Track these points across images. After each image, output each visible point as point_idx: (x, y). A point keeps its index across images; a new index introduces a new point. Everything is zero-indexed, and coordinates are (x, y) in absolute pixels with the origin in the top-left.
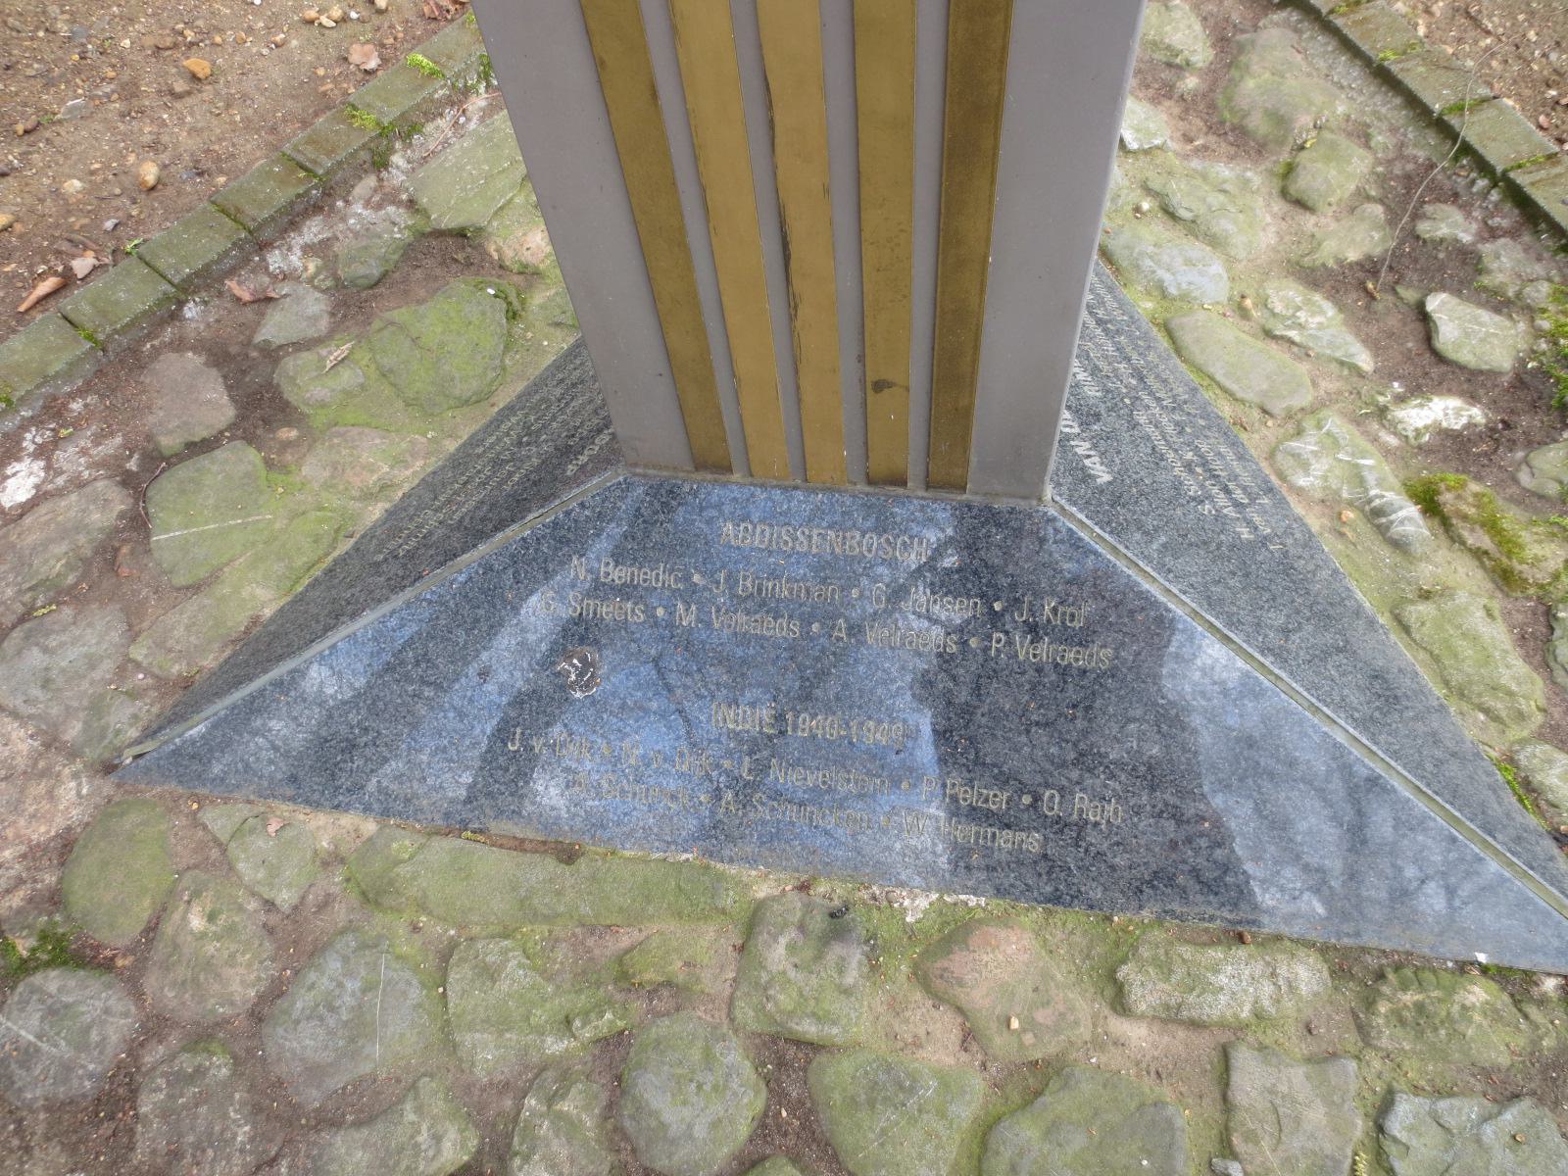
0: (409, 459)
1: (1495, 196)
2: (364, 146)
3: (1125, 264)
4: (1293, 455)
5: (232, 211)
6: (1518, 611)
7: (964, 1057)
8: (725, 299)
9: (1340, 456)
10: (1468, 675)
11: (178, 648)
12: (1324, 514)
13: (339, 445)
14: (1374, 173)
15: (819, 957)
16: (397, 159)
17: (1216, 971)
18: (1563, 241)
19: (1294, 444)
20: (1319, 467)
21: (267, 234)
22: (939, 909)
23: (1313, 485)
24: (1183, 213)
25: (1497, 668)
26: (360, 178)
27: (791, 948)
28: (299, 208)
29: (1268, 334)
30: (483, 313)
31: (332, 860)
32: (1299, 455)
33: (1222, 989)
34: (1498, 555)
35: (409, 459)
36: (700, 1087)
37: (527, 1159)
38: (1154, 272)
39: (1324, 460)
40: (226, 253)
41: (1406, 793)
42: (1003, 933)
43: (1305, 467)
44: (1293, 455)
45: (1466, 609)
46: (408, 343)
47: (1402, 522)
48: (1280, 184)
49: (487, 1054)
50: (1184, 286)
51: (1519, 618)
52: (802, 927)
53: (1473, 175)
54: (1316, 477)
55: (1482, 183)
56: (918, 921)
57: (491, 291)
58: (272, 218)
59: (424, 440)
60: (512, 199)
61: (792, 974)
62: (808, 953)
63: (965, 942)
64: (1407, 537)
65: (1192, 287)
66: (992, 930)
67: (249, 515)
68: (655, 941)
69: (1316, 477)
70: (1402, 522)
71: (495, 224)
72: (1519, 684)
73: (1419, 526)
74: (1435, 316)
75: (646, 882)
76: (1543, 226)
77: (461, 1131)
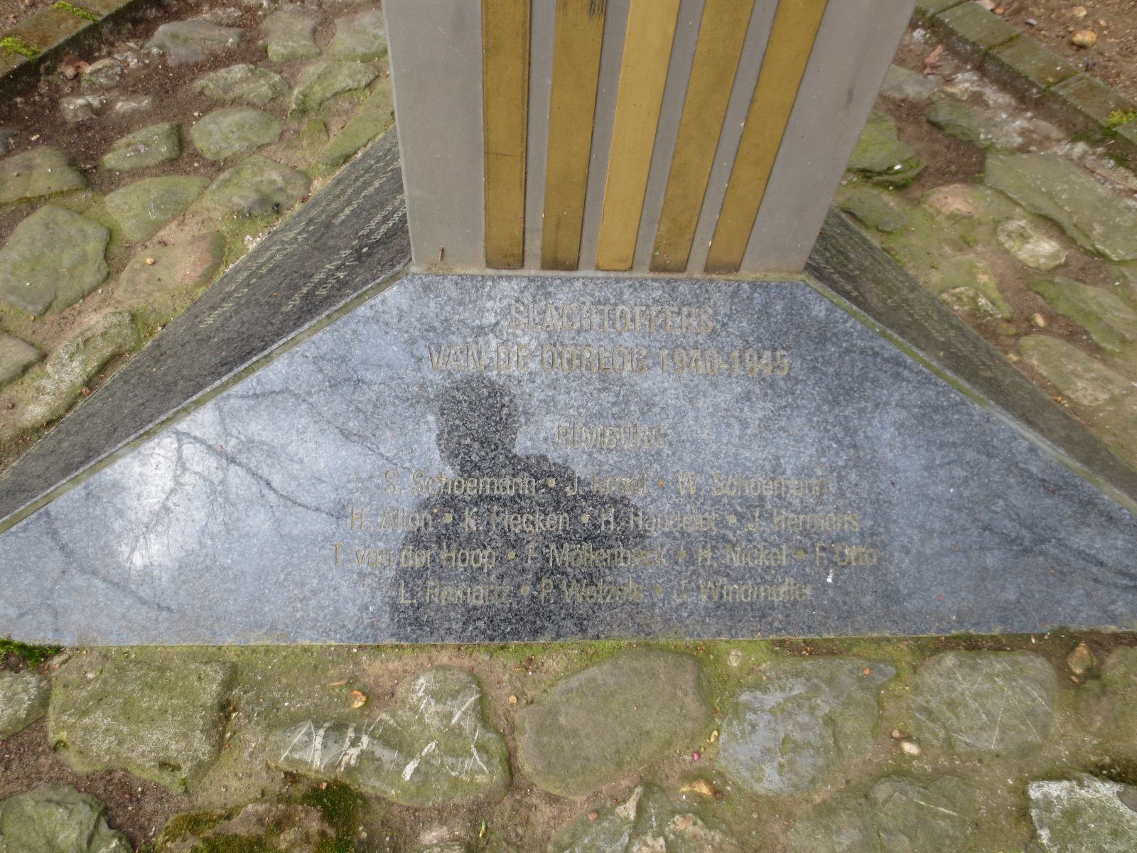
2: (1087, 117)
4: (458, 692)
5: (1010, 43)
6: (156, 812)
8: (775, 169)
9: (433, 745)
10: (126, 683)
12: (377, 684)
16: (1080, 147)
17: (82, 362)
19: (471, 700)
20: (431, 709)
21: (990, 67)
22: (245, 249)
23: (414, 691)
25: (114, 718)
26: (1060, 126)
27: (273, 182)
28: (1018, 84)
32: (454, 697)
33: (71, 361)
34: (217, 828)
36: (233, 132)
37: (251, 71)
38: (782, 689)
39: (436, 722)
40: (966, 41)
42: (200, 270)
43: (437, 696)
44: (458, 692)
45: (185, 736)
47: (309, 735)
50: (750, 716)
51: (149, 806)
52: (281, 190)
54: (420, 699)
56: (243, 241)
57: (898, 167)
58: (1003, 65)
60: (1018, 204)
61: (259, 179)
64: (292, 732)
65: (747, 728)
66: (206, 266)
68: (324, 137)
69: (420, 699)
70: (309, 735)
71: (989, 192)
72: (86, 729)
73: (294, 750)
77: (282, 55)
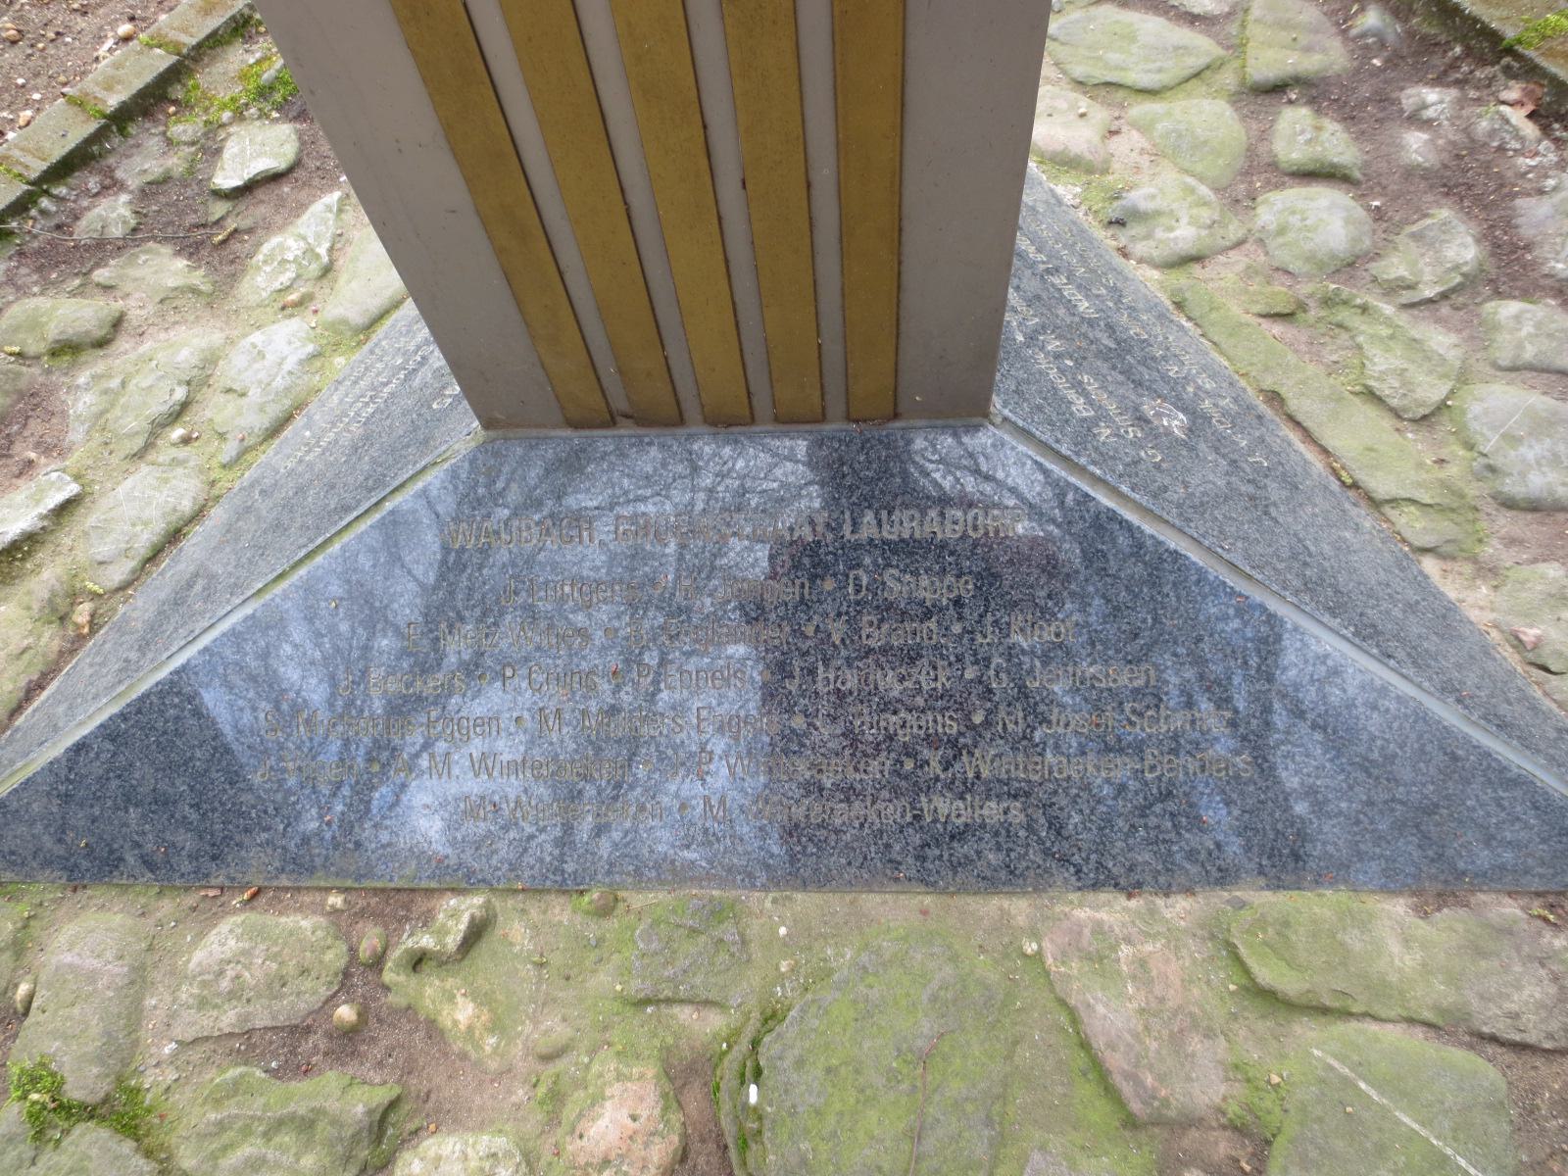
0: (1087, 932)
1: (61, 190)
3: (287, 402)
7: (1125, 129)
11: (1543, 972)
13: (1150, 1067)
14: (42, 294)
15: (1158, 213)
18: (114, 128)
24: (180, 394)
29: (327, 271)
30: (800, 1063)
31: (1488, 571)
35: (1087, 932)
41: (192, 651)
46: (930, 1143)
48: (90, 351)
49: (1441, 341)
53: (33, 212)
55: (45, 202)
59: (1046, 944)
62: (1163, 220)
63: (1063, 152)
67: (1345, 1080)
74: (246, 177)
75: (1231, 335)
76: (95, 148)
